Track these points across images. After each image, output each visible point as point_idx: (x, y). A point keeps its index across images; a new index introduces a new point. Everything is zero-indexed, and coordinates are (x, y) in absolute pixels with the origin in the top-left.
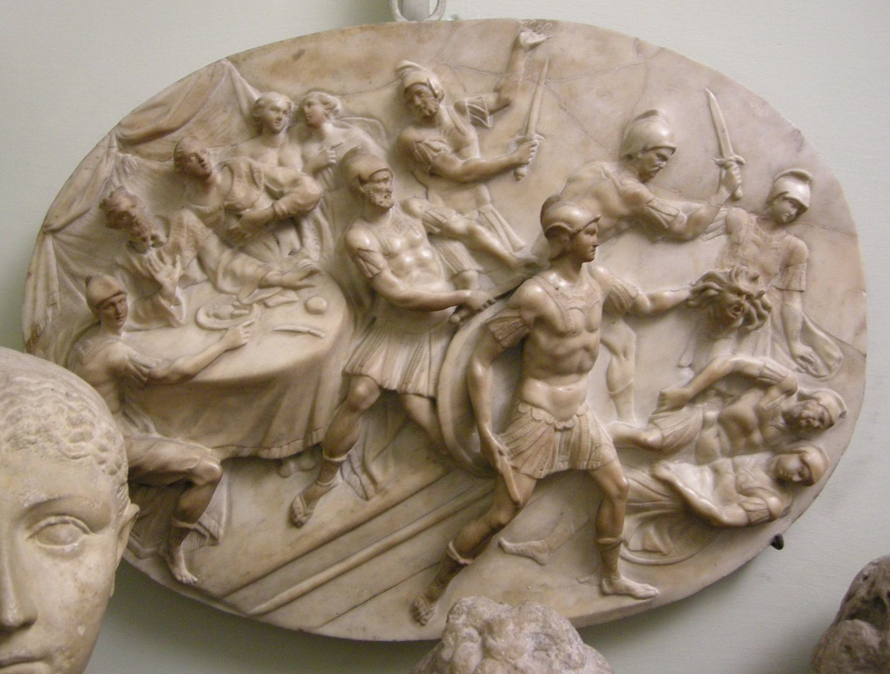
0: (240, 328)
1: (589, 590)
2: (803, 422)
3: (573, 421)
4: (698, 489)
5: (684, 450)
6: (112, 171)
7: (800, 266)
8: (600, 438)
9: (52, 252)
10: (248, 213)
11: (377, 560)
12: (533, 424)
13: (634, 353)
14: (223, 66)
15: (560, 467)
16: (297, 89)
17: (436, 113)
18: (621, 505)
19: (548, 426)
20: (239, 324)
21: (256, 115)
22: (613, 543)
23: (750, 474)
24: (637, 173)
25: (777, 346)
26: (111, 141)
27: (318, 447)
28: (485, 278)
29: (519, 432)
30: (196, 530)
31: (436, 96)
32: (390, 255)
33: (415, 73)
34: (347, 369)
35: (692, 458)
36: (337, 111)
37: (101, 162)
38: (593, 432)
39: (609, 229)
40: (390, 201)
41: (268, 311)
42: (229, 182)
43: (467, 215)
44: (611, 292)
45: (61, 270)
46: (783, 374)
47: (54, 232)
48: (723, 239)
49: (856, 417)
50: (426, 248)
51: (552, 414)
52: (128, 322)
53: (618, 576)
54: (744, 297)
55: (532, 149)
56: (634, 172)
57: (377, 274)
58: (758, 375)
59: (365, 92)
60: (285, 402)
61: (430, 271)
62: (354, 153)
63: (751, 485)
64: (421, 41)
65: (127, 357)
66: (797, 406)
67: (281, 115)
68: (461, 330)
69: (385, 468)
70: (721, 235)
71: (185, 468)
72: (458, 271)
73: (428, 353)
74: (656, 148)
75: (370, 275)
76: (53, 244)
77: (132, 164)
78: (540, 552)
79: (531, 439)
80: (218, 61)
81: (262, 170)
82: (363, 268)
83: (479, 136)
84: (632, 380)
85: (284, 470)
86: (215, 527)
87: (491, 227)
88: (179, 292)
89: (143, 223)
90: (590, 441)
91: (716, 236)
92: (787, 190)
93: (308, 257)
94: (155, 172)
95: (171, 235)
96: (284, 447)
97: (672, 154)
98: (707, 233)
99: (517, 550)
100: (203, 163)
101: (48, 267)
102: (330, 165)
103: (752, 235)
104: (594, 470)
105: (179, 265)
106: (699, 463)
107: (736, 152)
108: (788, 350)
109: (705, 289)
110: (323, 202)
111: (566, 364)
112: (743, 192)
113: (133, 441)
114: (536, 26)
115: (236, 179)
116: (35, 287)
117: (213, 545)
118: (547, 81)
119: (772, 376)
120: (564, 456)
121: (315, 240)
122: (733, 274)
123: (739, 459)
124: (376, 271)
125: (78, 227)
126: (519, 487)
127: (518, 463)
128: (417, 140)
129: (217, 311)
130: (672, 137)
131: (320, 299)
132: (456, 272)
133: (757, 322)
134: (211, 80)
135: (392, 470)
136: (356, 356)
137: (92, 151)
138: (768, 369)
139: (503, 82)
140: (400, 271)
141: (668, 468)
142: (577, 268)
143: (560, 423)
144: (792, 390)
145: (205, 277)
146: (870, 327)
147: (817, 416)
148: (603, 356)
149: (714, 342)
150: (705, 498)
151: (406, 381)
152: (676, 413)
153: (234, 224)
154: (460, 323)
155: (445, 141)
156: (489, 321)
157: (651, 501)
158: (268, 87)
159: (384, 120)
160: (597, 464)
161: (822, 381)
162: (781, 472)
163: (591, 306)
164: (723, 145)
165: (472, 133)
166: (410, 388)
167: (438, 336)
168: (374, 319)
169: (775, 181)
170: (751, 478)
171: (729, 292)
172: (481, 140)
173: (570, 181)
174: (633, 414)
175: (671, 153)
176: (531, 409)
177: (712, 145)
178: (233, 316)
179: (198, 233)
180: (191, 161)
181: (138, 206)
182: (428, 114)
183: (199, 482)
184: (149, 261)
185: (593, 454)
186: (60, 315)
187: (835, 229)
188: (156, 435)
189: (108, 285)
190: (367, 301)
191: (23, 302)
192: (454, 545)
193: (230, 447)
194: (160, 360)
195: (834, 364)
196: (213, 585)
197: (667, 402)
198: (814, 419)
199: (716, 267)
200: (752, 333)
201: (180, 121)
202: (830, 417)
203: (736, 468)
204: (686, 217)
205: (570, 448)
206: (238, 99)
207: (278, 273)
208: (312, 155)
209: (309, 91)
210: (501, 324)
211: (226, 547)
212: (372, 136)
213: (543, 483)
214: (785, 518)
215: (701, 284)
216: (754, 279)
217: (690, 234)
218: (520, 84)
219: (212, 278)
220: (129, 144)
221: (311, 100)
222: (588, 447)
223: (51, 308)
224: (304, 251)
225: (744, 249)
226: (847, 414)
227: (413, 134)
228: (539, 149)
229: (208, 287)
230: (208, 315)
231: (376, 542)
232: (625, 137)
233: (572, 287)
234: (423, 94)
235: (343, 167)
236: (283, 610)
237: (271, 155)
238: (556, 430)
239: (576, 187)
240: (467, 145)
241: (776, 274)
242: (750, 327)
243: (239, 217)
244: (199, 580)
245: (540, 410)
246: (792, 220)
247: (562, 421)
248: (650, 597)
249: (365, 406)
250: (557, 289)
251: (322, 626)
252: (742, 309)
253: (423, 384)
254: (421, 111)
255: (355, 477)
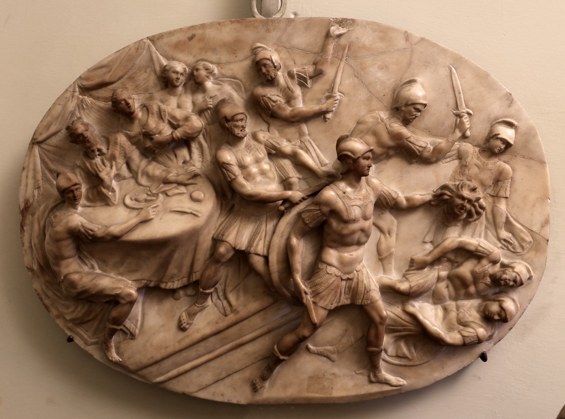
0: (149, 208)
1: (363, 379)
2: (502, 282)
3: (354, 274)
4: (433, 320)
5: (425, 295)
6: (75, 107)
7: (506, 181)
8: (370, 286)
9: (38, 156)
10: (157, 137)
11: (231, 353)
12: (327, 276)
13: (395, 232)
14: (145, 43)
15: (345, 302)
16: (191, 59)
17: (275, 78)
18: (382, 328)
19: (337, 277)
20: (150, 206)
21: (164, 76)
22: (377, 351)
23: (467, 312)
24: (401, 119)
25: (489, 233)
26: (74, 88)
27: (196, 284)
28: (302, 182)
29: (318, 281)
30: (121, 330)
31: (275, 67)
32: (242, 167)
33: (265, 52)
34: (215, 237)
35: (431, 300)
36: (215, 74)
37: (68, 101)
38: (365, 282)
39: (381, 155)
40: (244, 133)
41: (168, 198)
42: (146, 116)
43: (293, 143)
44: (381, 195)
45: (43, 167)
46: (491, 251)
47: (39, 143)
48: (456, 162)
49: (540, 280)
50: (266, 163)
51: (339, 270)
52: (83, 201)
53: (380, 371)
54: (466, 201)
55: (335, 102)
56: (399, 119)
57: (234, 179)
58: (474, 250)
59: (233, 62)
60: (176, 256)
61: (268, 178)
62: (223, 102)
63: (466, 319)
64: (268, 31)
65: (80, 224)
66: (499, 271)
67: (179, 76)
68: (284, 216)
69: (238, 297)
70: (455, 160)
71: (114, 293)
72: (285, 178)
73: (265, 228)
74: (414, 104)
75: (229, 179)
76: (38, 149)
77: (87, 103)
78: (332, 353)
79: (326, 285)
80: (142, 40)
81: (166, 110)
82: (226, 174)
83: (302, 93)
84: (393, 250)
85: (177, 295)
86: (133, 328)
87: (307, 151)
88: (114, 184)
89: (92, 141)
90: (364, 287)
91: (452, 161)
92: (499, 133)
93: (194, 166)
94: (102, 108)
95: (110, 149)
96: (175, 282)
97: (424, 108)
98: (445, 159)
99: (318, 352)
100: (129, 105)
101: (35, 164)
102: (209, 108)
103: (475, 161)
104: (365, 305)
105: (114, 168)
106: (435, 303)
107: (467, 107)
108: (496, 235)
109: (442, 194)
110: (205, 132)
111: (349, 240)
112: (470, 133)
113: (83, 275)
114: (341, 22)
115: (150, 115)
116: (27, 177)
117: (132, 339)
118: (346, 58)
119: (483, 251)
120: (347, 296)
121: (199, 154)
122: (460, 186)
123: (460, 302)
124: (233, 177)
125: (54, 141)
126: (317, 315)
127: (317, 300)
128: (262, 95)
129: (137, 197)
130: (425, 97)
131: (200, 192)
132: (284, 178)
133: (475, 216)
134: (137, 52)
135: (242, 299)
136: (221, 228)
137: (63, 93)
138: (481, 246)
139: (318, 58)
140: (249, 177)
141: (414, 306)
142: (358, 180)
143: (345, 275)
144: (496, 261)
145: (131, 175)
146: (551, 221)
147: (512, 279)
148: (375, 234)
149: (446, 228)
150: (436, 326)
151: (250, 245)
152: (420, 272)
153: (148, 144)
154: (284, 211)
155: (281, 95)
156: (301, 211)
157: (401, 327)
158: (172, 57)
159: (244, 80)
160: (367, 302)
161: (518, 256)
162: (487, 313)
163: (366, 204)
164: (458, 102)
165: (298, 91)
166: (252, 250)
167: (272, 219)
168: (233, 206)
169: (492, 126)
170: (467, 315)
171: (457, 198)
172: (304, 95)
173: (359, 123)
174: (393, 271)
175: (424, 107)
176: (326, 267)
177: (452, 102)
178: (146, 201)
179: (127, 148)
180: (122, 104)
181: (90, 130)
182: (270, 78)
183: (123, 302)
184: (96, 164)
185: (365, 296)
186: (42, 195)
187: (531, 158)
188: (98, 271)
189: (69, 179)
190: (229, 195)
191: (20, 185)
192: (277, 347)
193: (143, 281)
194: (100, 227)
195: (526, 245)
196: (131, 364)
197: (415, 265)
198: (509, 280)
199: (450, 180)
200: (472, 223)
201: (117, 77)
202: (521, 280)
203: (458, 308)
204: (432, 148)
205: (351, 291)
206: (153, 64)
207: (176, 175)
208: (198, 102)
209: (198, 61)
210: (308, 214)
211: (139, 341)
212: (236, 91)
213: (332, 313)
214: (489, 341)
215: (439, 192)
216: (474, 190)
217: (434, 159)
218: (329, 60)
219: (135, 177)
220: (85, 90)
221: (198, 67)
222: (362, 291)
223: (37, 190)
224: (192, 161)
225: (469, 170)
226: (533, 278)
227: (261, 91)
228: (340, 102)
229: (132, 182)
230: (131, 199)
231: (231, 342)
232: (395, 96)
233: (355, 192)
234: (267, 66)
235: (216, 110)
236: (174, 381)
237: (173, 101)
238: (342, 280)
239: (361, 127)
240: (295, 98)
241: (490, 186)
242: (471, 220)
243: (152, 139)
244: (123, 360)
245: (332, 267)
246: (501, 152)
247: (347, 274)
248: (400, 386)
249: (224, 260)
250: (344, 193)
251: (197, 392)
252: (465, 208)
253: (260, 247)
254: (266, 76)
255: (219, 301)
